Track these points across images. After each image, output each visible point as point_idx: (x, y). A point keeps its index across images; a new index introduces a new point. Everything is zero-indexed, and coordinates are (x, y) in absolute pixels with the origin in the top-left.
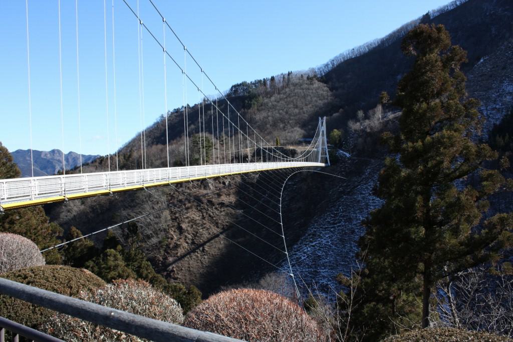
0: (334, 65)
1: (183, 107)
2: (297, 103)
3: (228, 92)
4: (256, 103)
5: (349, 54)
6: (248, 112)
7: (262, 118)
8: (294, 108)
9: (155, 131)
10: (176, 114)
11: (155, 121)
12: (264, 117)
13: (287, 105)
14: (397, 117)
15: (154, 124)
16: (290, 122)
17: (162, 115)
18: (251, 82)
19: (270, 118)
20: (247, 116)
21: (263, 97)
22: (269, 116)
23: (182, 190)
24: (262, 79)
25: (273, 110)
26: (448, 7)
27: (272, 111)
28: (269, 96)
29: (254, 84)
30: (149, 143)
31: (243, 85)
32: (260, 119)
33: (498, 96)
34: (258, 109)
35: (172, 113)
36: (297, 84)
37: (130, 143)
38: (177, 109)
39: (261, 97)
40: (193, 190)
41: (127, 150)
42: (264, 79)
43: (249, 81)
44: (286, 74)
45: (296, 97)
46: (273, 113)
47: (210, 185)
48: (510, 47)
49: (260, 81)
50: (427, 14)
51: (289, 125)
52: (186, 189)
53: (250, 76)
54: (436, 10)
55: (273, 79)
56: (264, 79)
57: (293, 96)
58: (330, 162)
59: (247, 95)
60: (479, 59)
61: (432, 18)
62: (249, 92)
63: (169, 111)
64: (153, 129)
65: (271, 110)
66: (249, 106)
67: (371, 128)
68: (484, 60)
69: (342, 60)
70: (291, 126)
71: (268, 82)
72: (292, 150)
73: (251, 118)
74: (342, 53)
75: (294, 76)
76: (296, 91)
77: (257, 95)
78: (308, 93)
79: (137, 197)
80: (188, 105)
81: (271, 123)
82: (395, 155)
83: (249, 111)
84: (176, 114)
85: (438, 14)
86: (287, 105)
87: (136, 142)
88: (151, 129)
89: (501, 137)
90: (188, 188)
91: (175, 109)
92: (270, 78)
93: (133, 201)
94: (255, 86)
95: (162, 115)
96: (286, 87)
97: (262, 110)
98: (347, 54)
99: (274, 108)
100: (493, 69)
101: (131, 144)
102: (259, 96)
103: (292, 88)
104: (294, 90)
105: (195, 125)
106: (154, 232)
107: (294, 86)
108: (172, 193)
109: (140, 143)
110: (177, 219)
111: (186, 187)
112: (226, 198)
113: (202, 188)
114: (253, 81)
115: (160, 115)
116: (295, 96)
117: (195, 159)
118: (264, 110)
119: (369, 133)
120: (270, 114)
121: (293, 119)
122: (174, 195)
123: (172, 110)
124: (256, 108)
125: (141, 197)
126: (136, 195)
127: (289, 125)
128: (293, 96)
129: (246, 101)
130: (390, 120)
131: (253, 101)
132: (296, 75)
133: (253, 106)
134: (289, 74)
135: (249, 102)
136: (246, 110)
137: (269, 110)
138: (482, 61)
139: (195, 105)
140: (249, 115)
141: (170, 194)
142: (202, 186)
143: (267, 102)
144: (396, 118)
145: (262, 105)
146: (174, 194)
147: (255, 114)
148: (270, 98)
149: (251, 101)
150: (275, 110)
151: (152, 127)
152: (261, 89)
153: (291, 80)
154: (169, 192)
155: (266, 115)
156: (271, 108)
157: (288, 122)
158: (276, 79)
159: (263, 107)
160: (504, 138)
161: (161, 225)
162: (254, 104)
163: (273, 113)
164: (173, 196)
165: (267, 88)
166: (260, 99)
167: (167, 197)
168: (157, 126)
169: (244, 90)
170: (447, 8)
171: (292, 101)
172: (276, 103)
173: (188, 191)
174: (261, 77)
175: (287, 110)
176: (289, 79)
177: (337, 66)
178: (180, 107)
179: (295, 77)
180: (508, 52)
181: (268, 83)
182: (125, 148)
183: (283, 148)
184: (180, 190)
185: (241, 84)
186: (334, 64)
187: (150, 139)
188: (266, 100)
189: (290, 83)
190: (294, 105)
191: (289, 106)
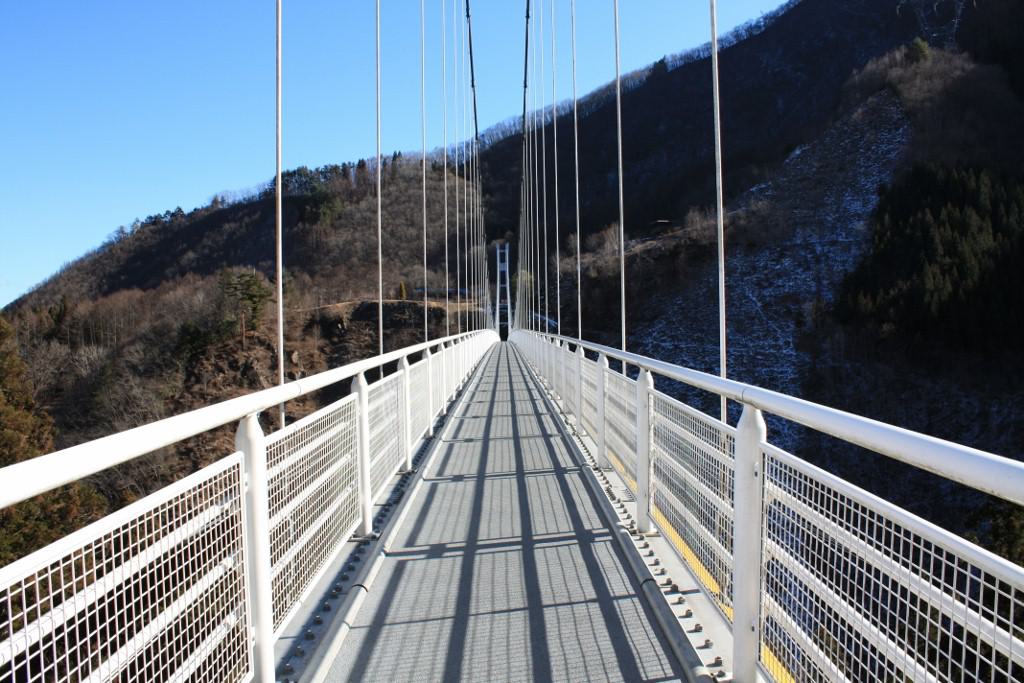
0: (484, 146)
1: (168, 212)
2: (412, 216)
3: (267, 187)
4: (328, 212)
5: (514, 125)
6: (311, 230)
7: (341, 243)
8: (408, 226)
9: (106, 262)
10: (152, 227)
11: (106, 240)
12: (347, 242)
13: (394, 219)
14: (649, 251)
15: (104, 246)
16: (400, 253)
17: (122, 228)
18: (317, 170)
19: (358, 244)
20: (310, 238)
21: (343, 202)
22: (355, 240)
23: (201, 389)
24: (340, 164)
25: (365, 227)
26: (699, 51)
27: (362, 230)
28: (355, 198)
29: (322, 173)
30: (91, 287)
31: (300, 175)
32: (337, 246)
33: (838, 219)
34: (332, 225)
35: (144, 225)
36: (412, 179)
37: (46, 284)
38: (156, 217)
39: (338, 199)
40: (225, 390)
41: (40, 299)
42: (344, 164)
43: (311, 167)
44: (388, 157)
45: (412, 205)
46: (363, 235)
47: (262, 378)
48: (845, 132)
49: (335, 168)
50: (662, 62)
51: (397, 260)
52: (208, 387)
53: (315, 160)
54: (678, 56)
55: (362, 164)
56: (344, 164)
57: (404, 202)
58: (341, 362)
59: (309, 194)
60: (791, 149)
61: (670, 69)
62: (313, 189)
63: (138, 221)
64: (101, 257)
65: (359, 228)
66: (315, 218)
67: (599, 271)
68: (803, 152)
69: (501, 137)
70: (402, 262)
71: (352, 170)
72: (434, 309)
73: (317, 242)
74: (501, 122)
75: (404, 162)
76: (411, 191)
77: (330, 196)
78: (434, 197)
79: (97, 404)
80: (180, 210)
81: (360, 253)
82: (649, 327)
83: (315, 227)
84: (152, 227)
85: (682, 63)
86: (394, 219)
87: (62, 283)
88: (97, 257)
89: (869, 297)
90: (215, 385)
91: (150, 218)
92: (356, 162)
93: (86, 412)
94: (325, 177)
95: (122, 228)
96: (389, 184)
97: (341, 226)
98: (510, 126)
99: (366, 224)
100: (822, 170)
101: (49, 288)
102: (334, 196)
103: (403, 185)
104: (406, 190)
105: (195, 251)
106: (138, 482)
107: (407, 182)
108: (177, 396)
109: (430, 230)
110: (192, 454)
111: (209, 382)
112: (298, 408)
113: (246, 386)
114: (321, 167)
115: (116, 227)
116: (409, 201)
117: (228, 322)
118: (346, 227)
119: (595, 279)
120: (357, 235)
121: (404, 249)
122: (181, 400)
123: (143, 219)
124: (328, 221)
125: (106, 402)
126: (96, 399)
127: (397, 260)
128: (404, 202)
129: (308, 207)
130: (636, 255)
131: (323, 209)
132: (409, 160)
133: (322, 217)
134: (396, 157)
135: (314, 210)
136: (307, 226)
137: (355, 229)
138: (798, 152)
139: (195, 210)
140: (315, 237)
141: (173, 397)
142: (246, 382)
143: (351, 211)
144: (648, 252)
145: (340, 218)
146: (182, 397)
147: (326, 234)
148: (358, 202)
149: (318, 208)
150: (369, 228)
151: (98, 253)
152: (338, 184)
153: (400, 170)
154: (171, 394)
155: (350, 237)
156: (359, 224)
157: (396, 254)
158: (369, 166)
159: (343, 221)
160: (874, 299)
161: (154, 467)
162: (324, 214)
163: (363, 235)
164: (180, 403)
165: (349, 183)
166: (336, 204)
167: (166, 404)
168: (110, 251)
169: (300, 185)
170: (697, 54)
171: (404, 213)
172: (368, 214)
173: (214, 391)
174: (338, 161)
175: (392, 230)
176: (394, 170)
177: (492, 147)
178: (162, 213)
179: (407, 164)
180: (843, 141)
181: (352, 172)
182: (36, 296)
183: (415, 304)
184: (196, 388)
185: (294, 172)
186: (484, 142)
187: (93, 278)
188: (349, 208)
189: (397, 176)
190: (407, 220)
191: (397, 221)
